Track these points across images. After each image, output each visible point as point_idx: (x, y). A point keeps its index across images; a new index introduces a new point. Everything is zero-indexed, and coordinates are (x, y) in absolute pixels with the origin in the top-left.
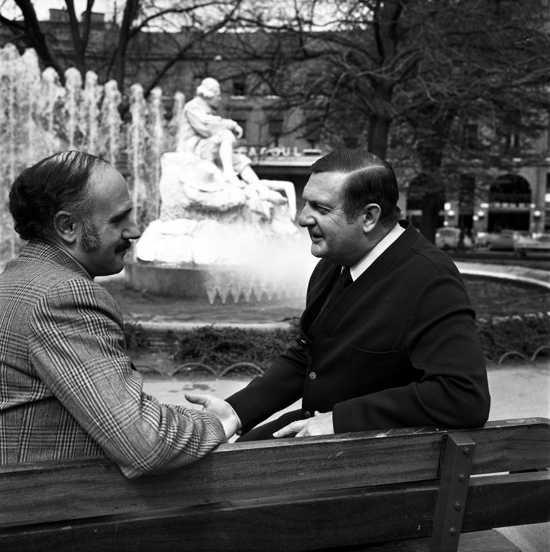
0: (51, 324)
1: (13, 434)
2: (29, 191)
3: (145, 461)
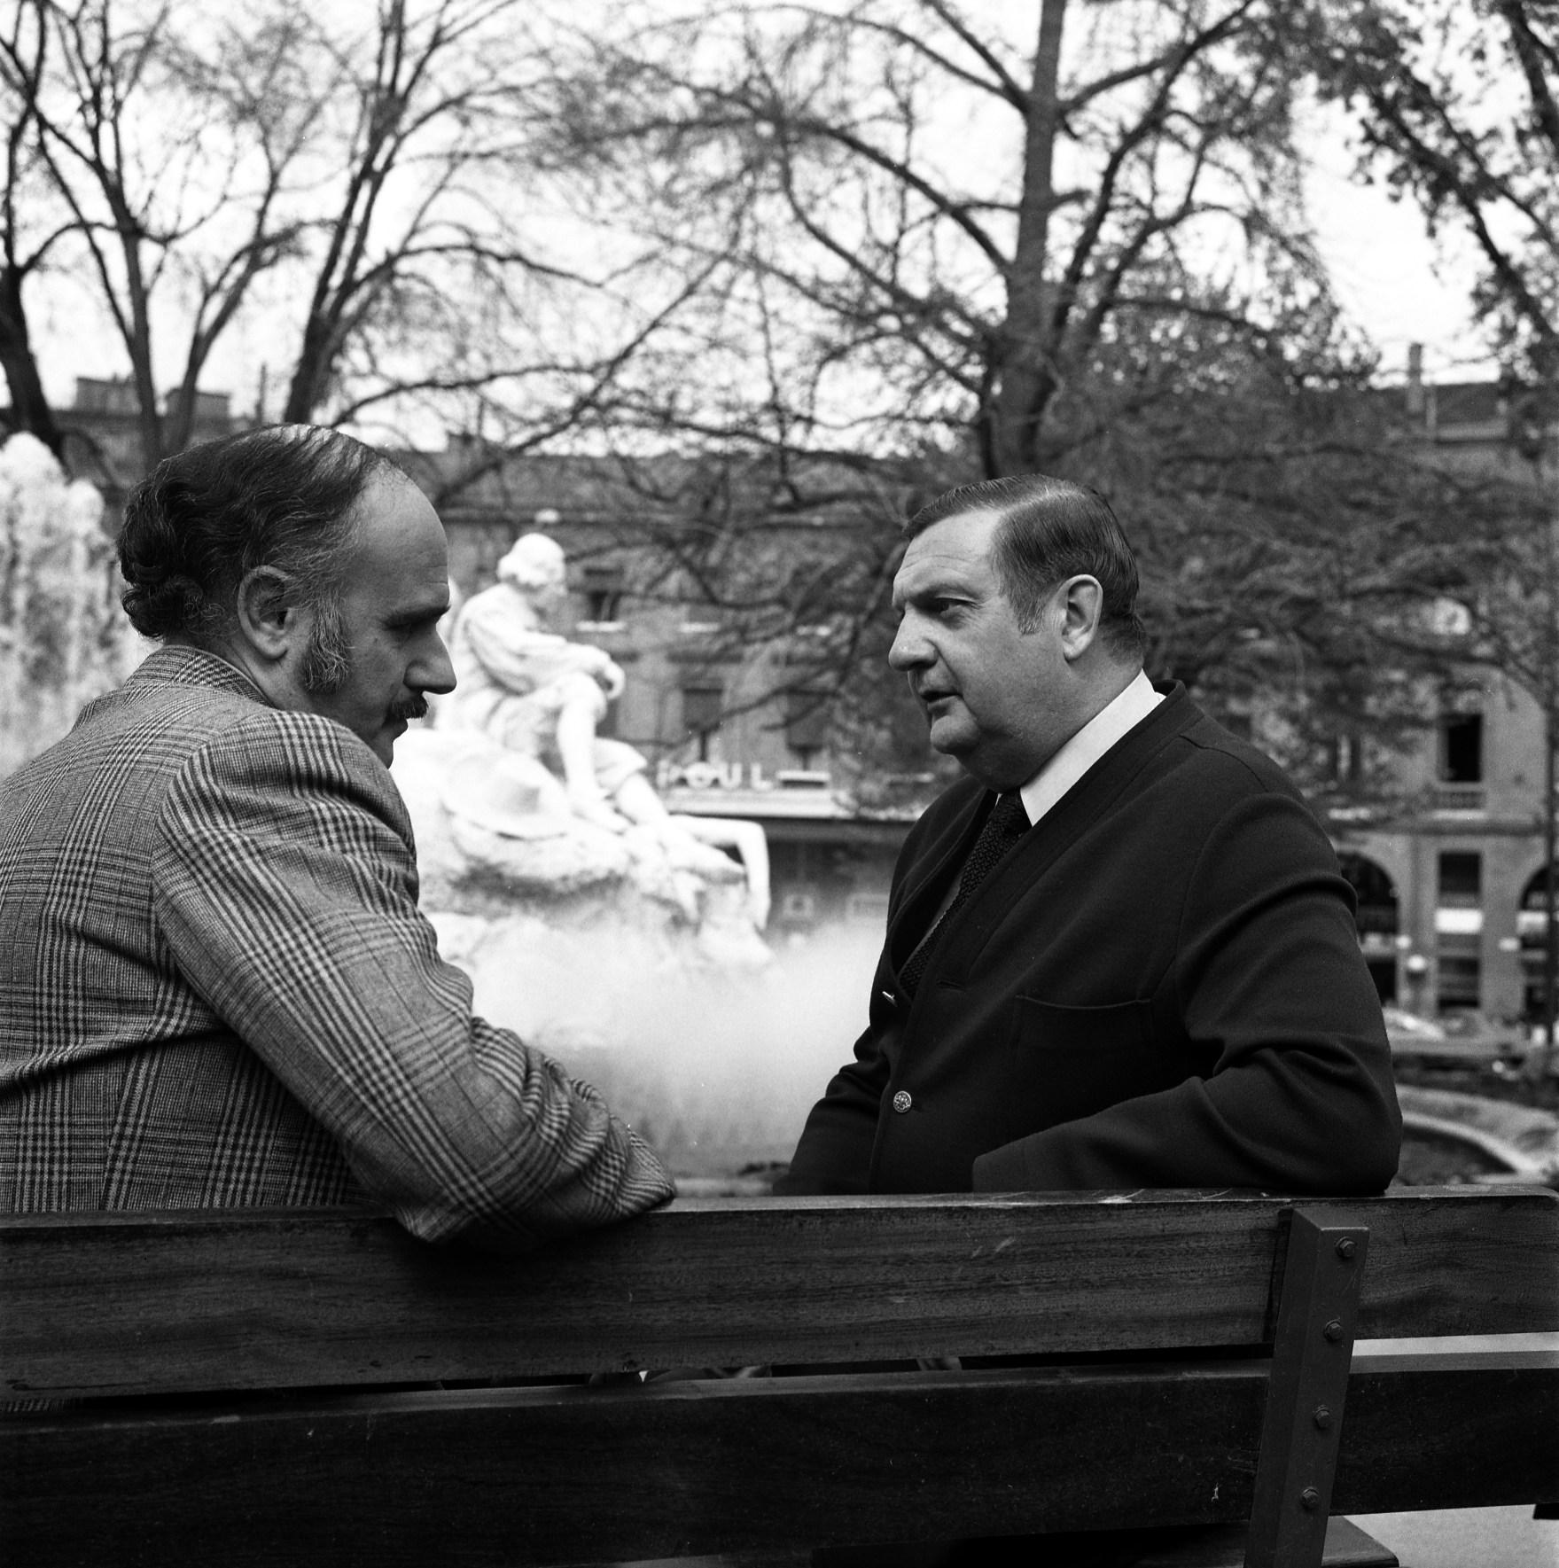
0: (220, 820)
1: (92, 1138)
2: (191, 498)
3: (481, 1180)
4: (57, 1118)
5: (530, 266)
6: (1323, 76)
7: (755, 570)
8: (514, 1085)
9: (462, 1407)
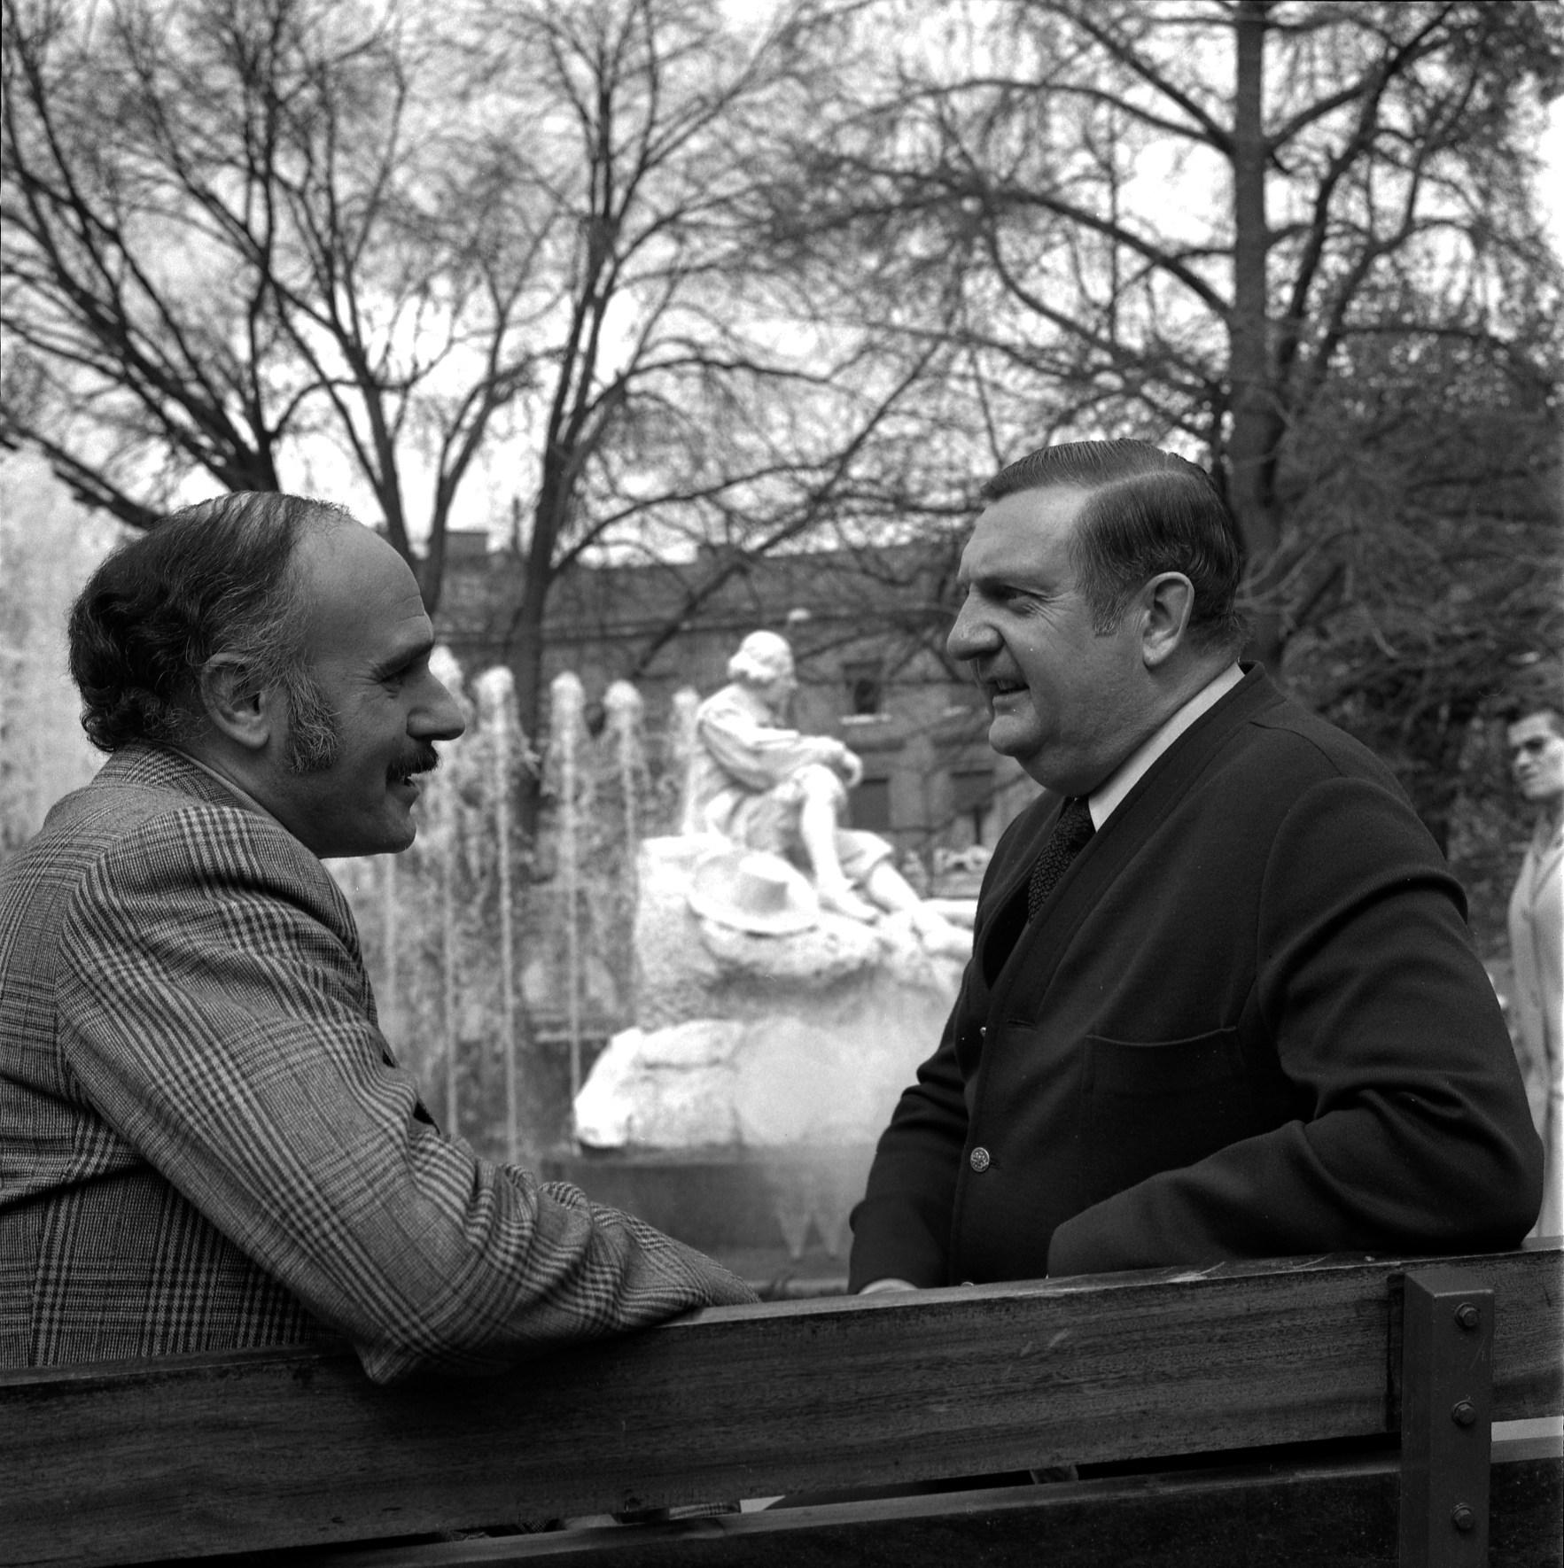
1: (15, 1285)
2: (121, 607)
3: (423, 1320)
5: (758, 371)
6: (1541, 73)
8: (456, 1210)
9: (474, 1559)
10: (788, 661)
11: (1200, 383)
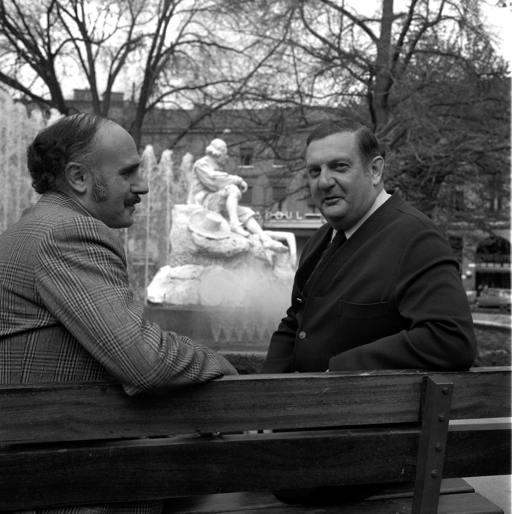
1: (17, 358)
2: (42, 147)
3: (145, 378)
4: (6, 351)
5: (219, 47)
7: (294, 147)
8: (156, 347)
10: (226, 149)
11: (367, 65)
